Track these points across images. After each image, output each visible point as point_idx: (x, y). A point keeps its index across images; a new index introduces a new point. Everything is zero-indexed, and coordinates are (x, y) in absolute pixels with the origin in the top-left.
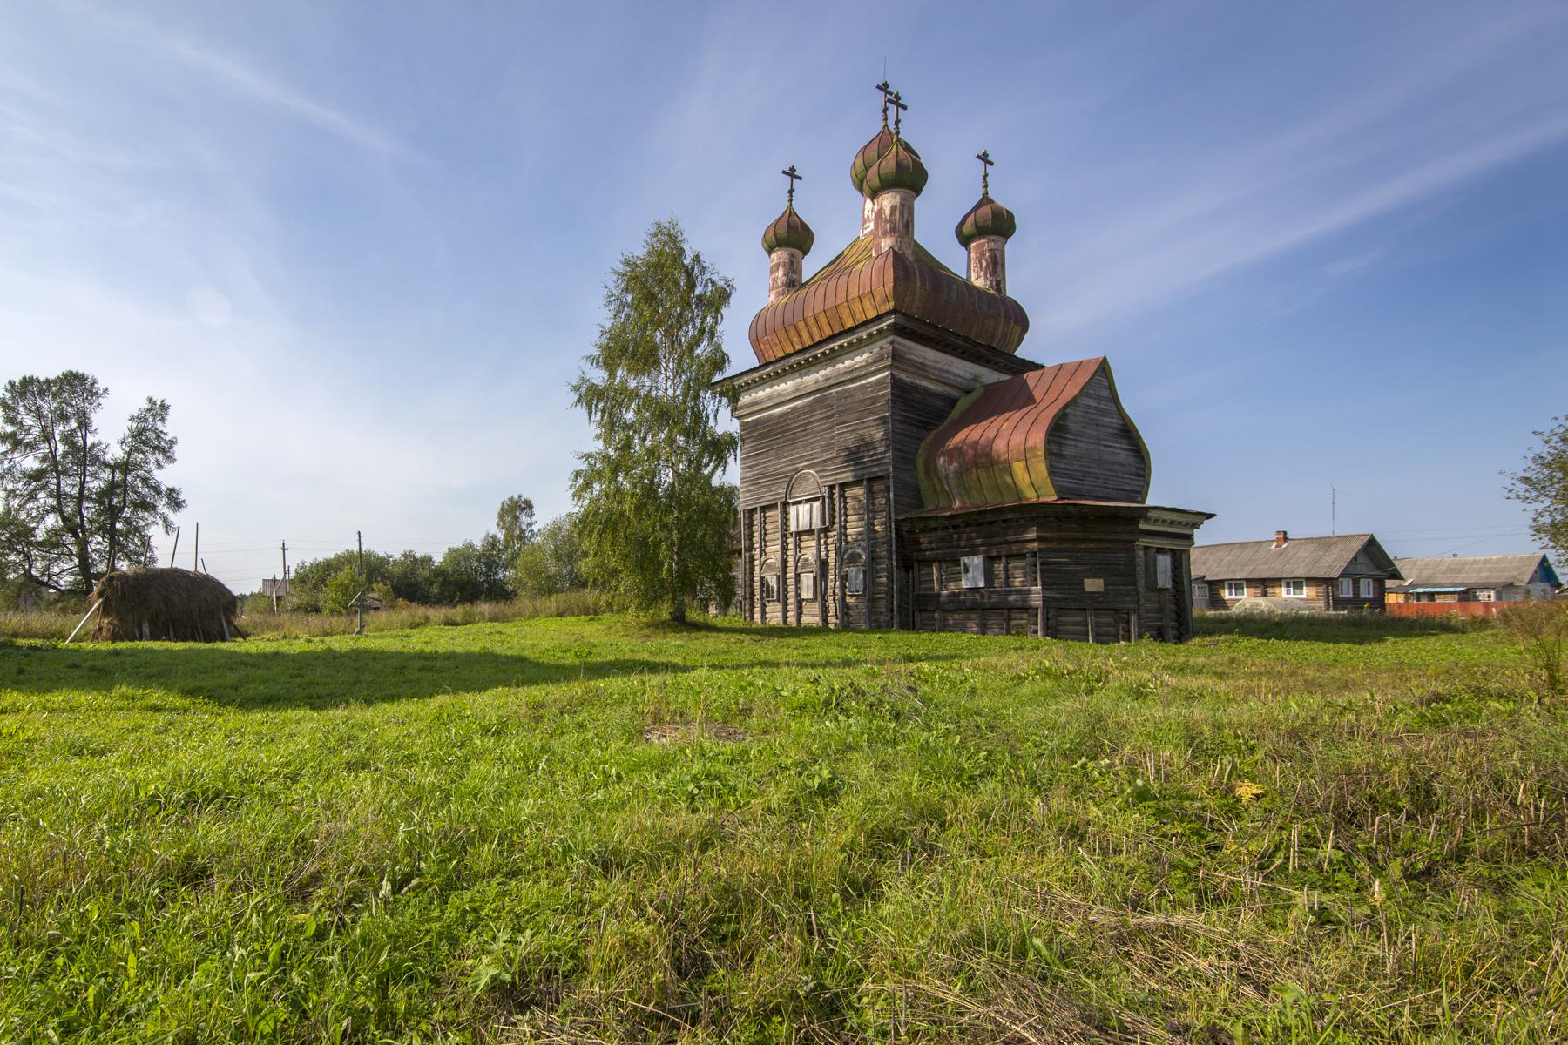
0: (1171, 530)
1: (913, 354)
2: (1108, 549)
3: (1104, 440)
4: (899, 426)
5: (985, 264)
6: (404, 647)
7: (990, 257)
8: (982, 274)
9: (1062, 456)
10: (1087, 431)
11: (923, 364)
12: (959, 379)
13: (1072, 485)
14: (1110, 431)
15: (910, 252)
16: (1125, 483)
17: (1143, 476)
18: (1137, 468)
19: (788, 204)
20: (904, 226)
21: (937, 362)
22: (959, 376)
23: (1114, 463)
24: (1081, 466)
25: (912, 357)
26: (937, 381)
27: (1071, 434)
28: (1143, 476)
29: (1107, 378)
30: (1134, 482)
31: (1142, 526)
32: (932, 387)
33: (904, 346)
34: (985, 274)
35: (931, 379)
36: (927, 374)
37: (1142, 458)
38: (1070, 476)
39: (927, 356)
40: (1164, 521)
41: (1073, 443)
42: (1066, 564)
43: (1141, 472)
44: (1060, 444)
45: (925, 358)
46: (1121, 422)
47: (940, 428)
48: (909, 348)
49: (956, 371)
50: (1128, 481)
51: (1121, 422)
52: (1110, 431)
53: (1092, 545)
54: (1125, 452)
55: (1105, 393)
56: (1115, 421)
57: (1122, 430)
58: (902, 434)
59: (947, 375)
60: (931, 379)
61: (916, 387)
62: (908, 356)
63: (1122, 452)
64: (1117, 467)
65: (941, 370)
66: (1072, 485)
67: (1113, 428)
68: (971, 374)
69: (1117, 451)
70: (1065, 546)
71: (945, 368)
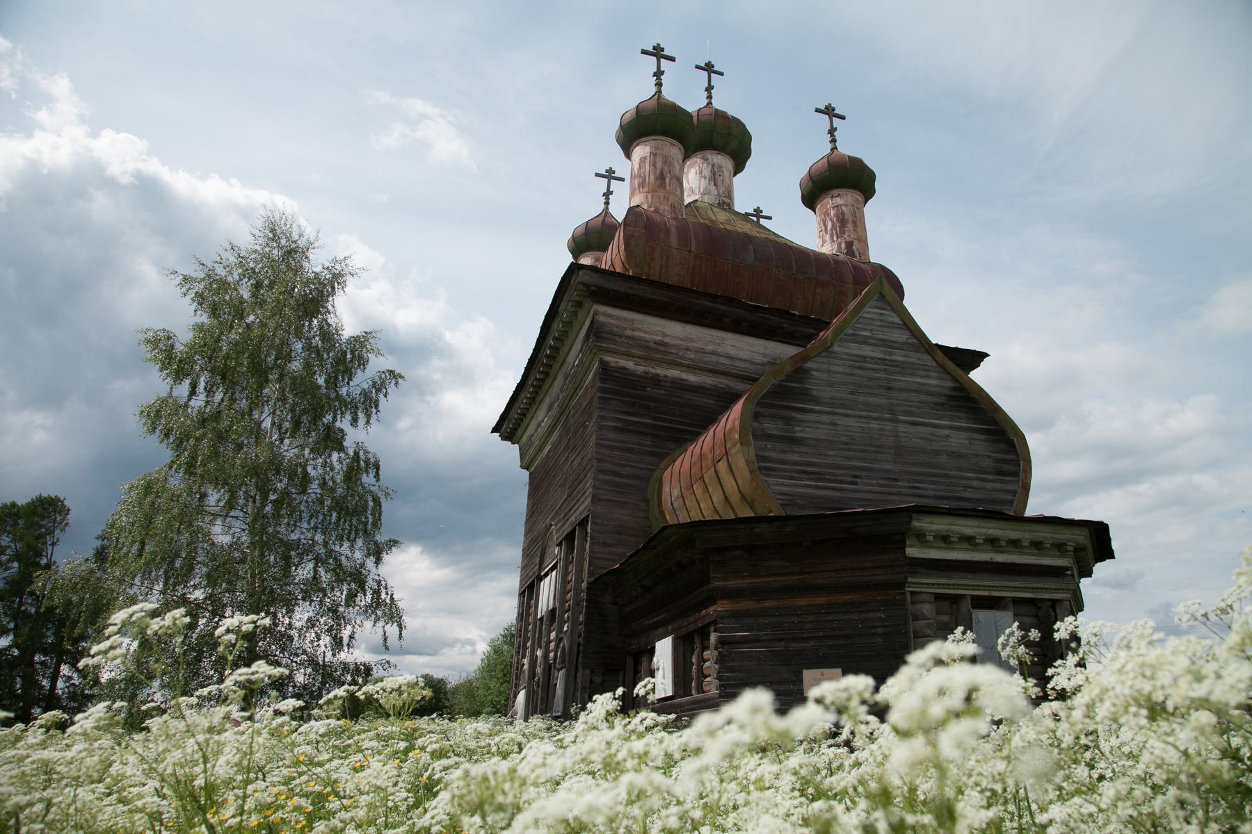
0: (1000, 558)
1: (639, 330)
3: (911, 414)
4: (612, 435)
5: (830, 225)
6: (1171, 733)
7: (837, 215)
8: (827, 237)
9: (794, 440)
10: (861, 398)
11: (662, 344)
12: (742, 365)
13: (823, 492)
14: (922, 397)
15: (667, 208)
16: (966, 487)
17: (1016, 474)
18: (997, 461)
19: (603, 206)
20: (656, 179)
21: (691, 340)
22: (740, 360)
23: (937, 453)
24: (850, 458)
25: (637, 334)
26: (689, 368)
27: (817, 401)
28: (1016, 474)
29: (893, 310)
30: (990, 485)
31: (913, 552)
32: (692, 378)
33: (619, 318)
34: (832, 236)
35: (683, 365)
36: (671, 357)
37: (1011, 444)
38: (820, 477)
40: (969, 540)
41: (824, 418)
42: (744, 641)
43: (1006, 467)
44: (789, 421)
45: (664, 335)
46: (949, 384)
48: (632, 321)
49: (733, 353)
50: (976, 483)
51: (949, 384)
52: (922, 397)
53: (821, 600)
54: (963, 435)
55: (901, 336)
56: (935, 382)
57: (951, 398)
58: (619, 449)
59: (714, 358)
60: (683, 365)
61: (656, 380)
62: (628, 333)
63: (954, 433)
64: (943, 459)
65: (701, 351)
66: (823, 492)
67: (928, 393)
68: (764, 355)
69: (947, 432)
70: (768, 604)
71: (710, 348)
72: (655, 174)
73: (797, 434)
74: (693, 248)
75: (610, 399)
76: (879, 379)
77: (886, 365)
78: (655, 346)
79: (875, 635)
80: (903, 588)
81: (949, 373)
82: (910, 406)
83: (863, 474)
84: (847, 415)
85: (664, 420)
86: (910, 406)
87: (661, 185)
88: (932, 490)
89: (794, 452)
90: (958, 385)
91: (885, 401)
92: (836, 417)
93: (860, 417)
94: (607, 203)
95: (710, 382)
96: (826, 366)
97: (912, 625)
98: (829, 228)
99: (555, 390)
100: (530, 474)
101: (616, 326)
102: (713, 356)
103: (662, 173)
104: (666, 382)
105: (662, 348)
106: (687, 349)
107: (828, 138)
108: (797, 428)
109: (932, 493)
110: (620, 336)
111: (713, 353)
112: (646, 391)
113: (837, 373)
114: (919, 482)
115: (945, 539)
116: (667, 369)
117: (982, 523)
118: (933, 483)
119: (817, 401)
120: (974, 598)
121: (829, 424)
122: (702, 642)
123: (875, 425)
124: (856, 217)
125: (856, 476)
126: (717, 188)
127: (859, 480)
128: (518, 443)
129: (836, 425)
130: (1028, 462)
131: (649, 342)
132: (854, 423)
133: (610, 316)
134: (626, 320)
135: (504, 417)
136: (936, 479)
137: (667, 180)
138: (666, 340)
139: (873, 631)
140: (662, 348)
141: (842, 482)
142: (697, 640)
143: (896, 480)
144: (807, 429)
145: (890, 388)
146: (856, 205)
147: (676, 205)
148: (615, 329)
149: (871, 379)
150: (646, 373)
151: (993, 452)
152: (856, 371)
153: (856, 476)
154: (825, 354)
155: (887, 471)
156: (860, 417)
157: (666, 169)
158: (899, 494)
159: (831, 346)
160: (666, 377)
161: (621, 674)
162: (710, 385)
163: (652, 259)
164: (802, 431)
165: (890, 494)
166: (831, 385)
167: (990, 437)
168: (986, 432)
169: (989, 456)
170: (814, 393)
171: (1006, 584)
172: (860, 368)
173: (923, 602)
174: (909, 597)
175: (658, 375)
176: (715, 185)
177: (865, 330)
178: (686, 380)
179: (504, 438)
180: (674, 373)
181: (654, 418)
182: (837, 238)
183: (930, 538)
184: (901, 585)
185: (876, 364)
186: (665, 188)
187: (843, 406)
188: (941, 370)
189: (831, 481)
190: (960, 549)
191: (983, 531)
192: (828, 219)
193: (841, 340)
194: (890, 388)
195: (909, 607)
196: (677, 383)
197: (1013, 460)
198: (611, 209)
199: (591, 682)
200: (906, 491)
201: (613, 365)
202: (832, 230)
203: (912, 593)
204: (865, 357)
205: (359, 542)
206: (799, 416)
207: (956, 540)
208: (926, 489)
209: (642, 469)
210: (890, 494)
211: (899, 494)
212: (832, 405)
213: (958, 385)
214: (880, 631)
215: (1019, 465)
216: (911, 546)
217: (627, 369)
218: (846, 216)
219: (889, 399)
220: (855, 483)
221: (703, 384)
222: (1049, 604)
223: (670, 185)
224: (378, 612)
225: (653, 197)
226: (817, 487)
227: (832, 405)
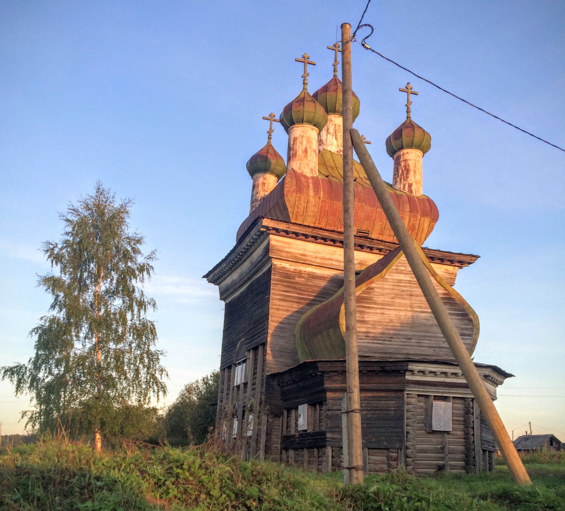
2: (382, 397)
10: (397, 300)
21: (319, 252)
25: (291, 250)
27: (376, 303)
31: (408, 377)
33: (283, 242)
37: (470, 320)
39: (307, 248)
41: (379, 311)
43: (466, 332)
45: (305, 250)
47: (324, 303)
48: (289, 243)
61: (300, 274)
62: (287, 250)
71: (328, 256)
72: (302, 149)
73: (366, 319)
74: (321, 197)
75: (277, 284)
76: (407, 291)
77: (410, 283)
78: (300, 256)
79: (390, 410)
80: (403, 392)
81: (443, 286)
82: (420, 304)
83: (395, 337)
84: (389, 309)
85: (304, 294)
86: (420, 304)
87: (305, 156)
88: (427, 343)
89: (363, 327)
90: (447, 292)
91: (409, 302)
92: (385, 310)
93: (396, 310)
94: (269, 138)
95: (328, 274)
96: (381, 286)
97: (406, 407)
98: (400, 174)
99: (245, 267)
100: (226, 305)
101: (281, 247)
102: (329, 261)
103: (306, 149)
104: (305, 274)
105: (304, 257)
106: (316, 258)
107: (363, 13)
108: (365, 316)
109: (427, 345)
110: (283, 252)
111: (330, 259)
112: (295, 280)
113: (387, 289)
114: (421, 340)
115: (423, 372)
116: (306, 267)
117: (440, 366)
118: (428, 340)
119: (376, 303)
120: (434, 396)
121: (380, 314)
122: (320, 408)
123: (402, 313)
124: (416, 167)
125: (391, 338)
126: (337, 141)
127: (392, 339)
128: (218, 285)
129: (384, 314)
130: (478, 330)
131: (297, 254)
132: (393, 313)
133: (278, 241)
134: (286, 243)
135: (210, 273)
136: (429, 338)
137: (309, 153)
138: (306, 253)
139: (390, 408)
140: (304, 257)
141: (384, 340)
142: (318, 407)
143: (410, 339)
144: (370, 316)
145: (411, 295)
146: (417, 159)
147: (313, 168)
148: (280, 248)
149: (403, 291)
150: (295, 270)
151: (460, 325)
152: (396, 287)
153: (391, 338)
154: (381, 279)
155: (406, 335)
156: (396, 310)
157: (308, 146)
158: (411, 346)
159: (385, 275)
160: (305, 271)
161: (281, 417)
162: (328, 275)
163: (299, 204)
164: (368, 317)
165: (407, 346)
166: (383, 295)
167: (460, 317)
168: (458, 315)
169: (458, 327)
170: (375, 299)
171: (450, 391)
172: (398, 286)
173: (413, 397)
174: (406, 396)
175: (301, 271)
176: (336, 139)
177: (402, 266)
178: (315, 273)
179: (210, 281)
180: (309, 269)
181: (299, 294)
182: (404, 181)
183: (416, 372)
184: (403, 391)
185: (406, 283)
186: (307, 158)
187: (388, 305)
188: (439, 285)
189: (379, 340)
190: (430, 376)
191: (441, 369)
192: (400, 168)
193: (390, 272)
194: (411, 295)
195: (406, 400)
196: (310, 275)
197: (470, 328)
198: (273, 143)
199: (268, 421)
200: (415, 344)
201: (278, 266)
202: (401, 175)
203: (407, 394)
204: (401, 280)
205: (268, 412)
206: (367, 310)
207: (428, 373)
208: (425, 343)
209: (293, 319)
210: (407, 346)
211: (411, 346)
212: (382, 304)
213: (447, 292)
214: (393, 409)
215: (473, 331)
216: (408, 375)
217: (286, 268)
218: (410, 167)
219: (410, 300)
220: (390, 341)
221: (324, 275)
222: (470, 399)
223: (310, 156)
224: (109, 361)
225: (300, 164)
226: (373, 343)
227: (382, 304)
